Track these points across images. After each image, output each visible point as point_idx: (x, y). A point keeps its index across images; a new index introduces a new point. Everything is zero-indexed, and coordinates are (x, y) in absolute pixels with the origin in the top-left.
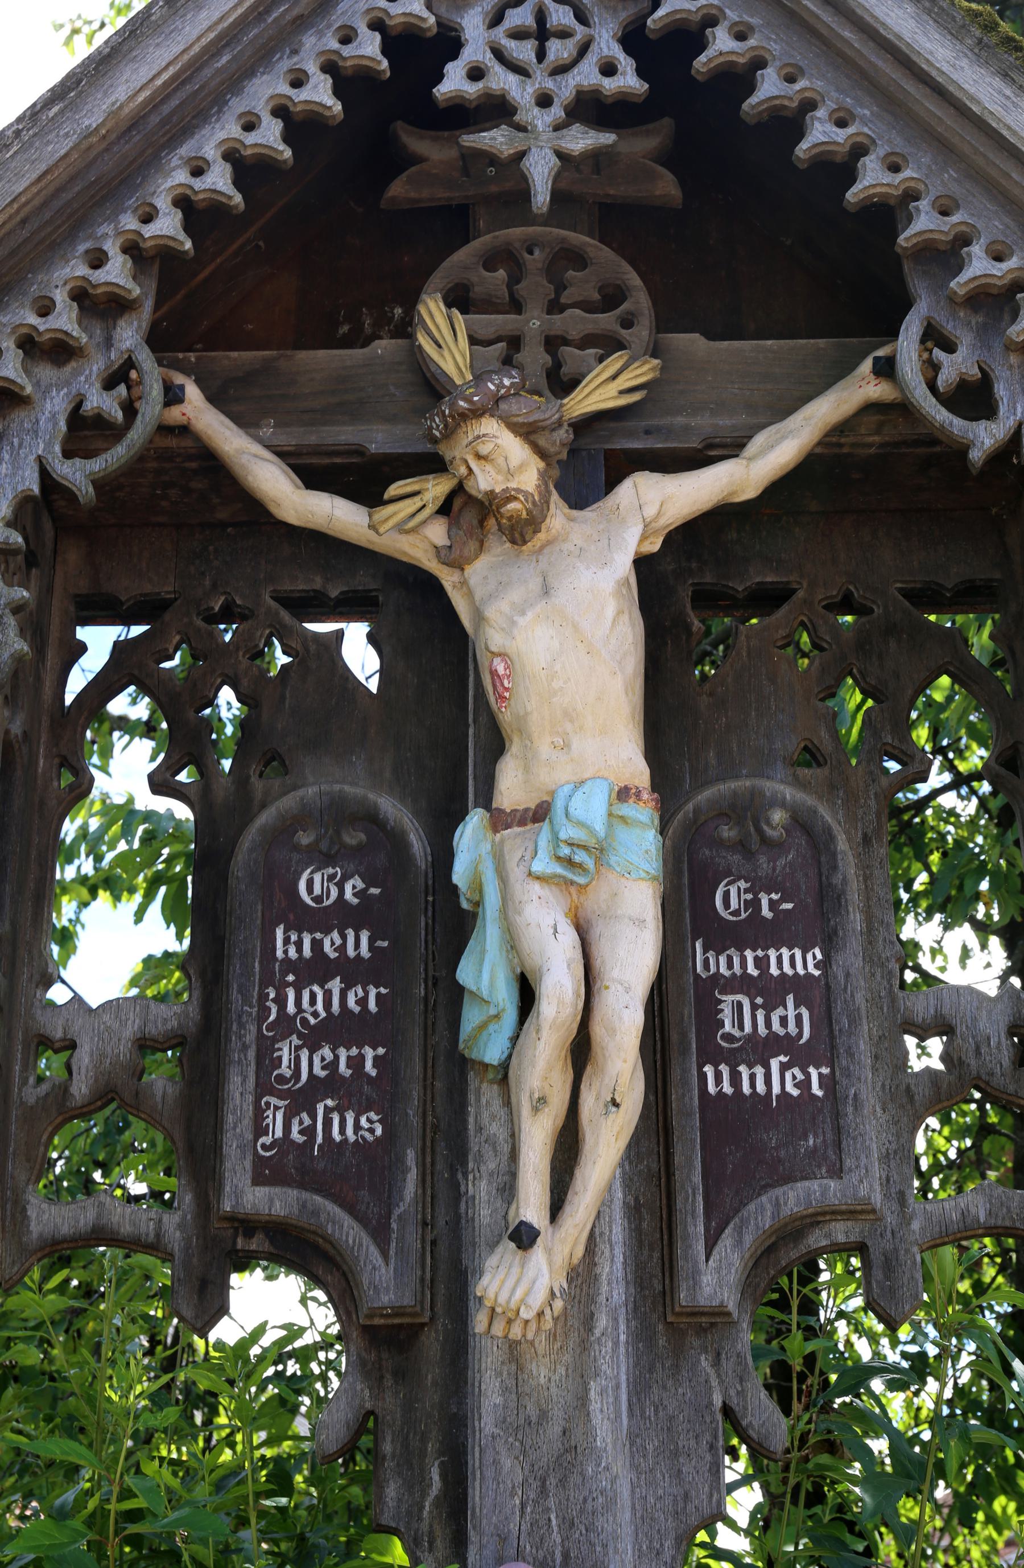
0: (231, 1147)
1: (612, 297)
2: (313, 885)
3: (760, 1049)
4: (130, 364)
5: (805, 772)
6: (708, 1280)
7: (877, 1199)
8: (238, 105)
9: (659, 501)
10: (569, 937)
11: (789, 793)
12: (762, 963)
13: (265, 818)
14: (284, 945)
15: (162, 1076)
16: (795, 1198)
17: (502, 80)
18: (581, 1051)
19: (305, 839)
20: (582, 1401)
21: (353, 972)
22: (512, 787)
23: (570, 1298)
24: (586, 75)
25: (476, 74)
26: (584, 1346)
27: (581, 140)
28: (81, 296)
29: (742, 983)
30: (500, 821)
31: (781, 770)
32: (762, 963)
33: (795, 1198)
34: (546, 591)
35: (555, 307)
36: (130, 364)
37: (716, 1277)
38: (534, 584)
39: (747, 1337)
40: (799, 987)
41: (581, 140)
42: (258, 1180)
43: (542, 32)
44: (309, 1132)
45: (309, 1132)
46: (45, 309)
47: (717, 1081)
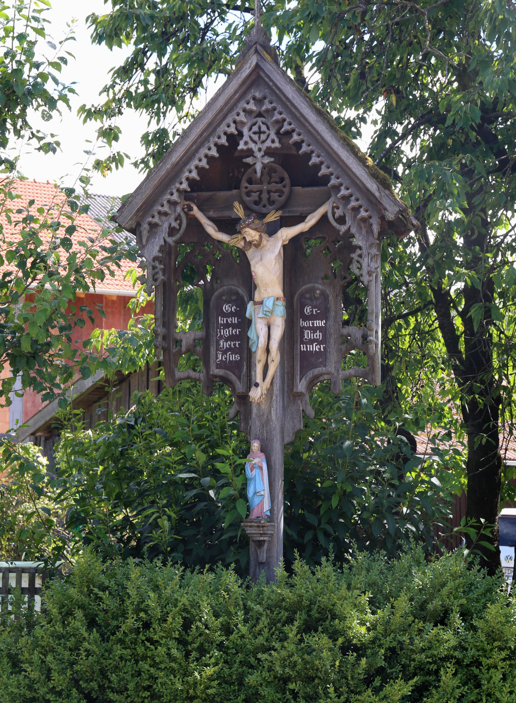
0: (212, 361)
1: (282, 180)
2: (226, 308)
3: (311, 342)
4: (179, 215)
5: (325, 281)
6: (299, 387)
7: (333, 371)
8: (197, 156)
9: (287, 233)
10: (265, 329)
11: (320, 287)
12: (313, 324)
13: (216, 293)
14: (221, 320)
15: (199, 349)
16: (317, 371)
17: (252, 145)
18: (268, 351)
19: (224, 298)
20: (270, 412)
21: (234, 326)
22: (257, 297)
23: (266, 395)
24: (268, 143)
25: (246, 143)
26: (271, 402)
27: (267, 160)
28: (169, 202)
29: (309, 328)
30: (255, 303)
31: (320, 281)
32: (313, 324)
33: (317, 371)
34: (261, 260)
35: (269, 183)
36: (179, 215)
37: (301, 386)
38: (259, 258)
39: (307, 397)
40: (320, 328)
41: (267, 160)
42: (217, 368)
43: (260, 132)
44: (226, 358)
45: (226, 358)
46: (162, 206)
47: (303, 348)
